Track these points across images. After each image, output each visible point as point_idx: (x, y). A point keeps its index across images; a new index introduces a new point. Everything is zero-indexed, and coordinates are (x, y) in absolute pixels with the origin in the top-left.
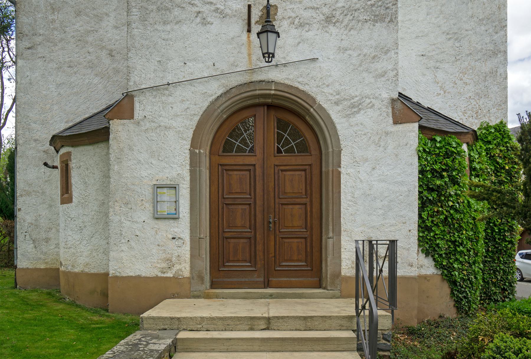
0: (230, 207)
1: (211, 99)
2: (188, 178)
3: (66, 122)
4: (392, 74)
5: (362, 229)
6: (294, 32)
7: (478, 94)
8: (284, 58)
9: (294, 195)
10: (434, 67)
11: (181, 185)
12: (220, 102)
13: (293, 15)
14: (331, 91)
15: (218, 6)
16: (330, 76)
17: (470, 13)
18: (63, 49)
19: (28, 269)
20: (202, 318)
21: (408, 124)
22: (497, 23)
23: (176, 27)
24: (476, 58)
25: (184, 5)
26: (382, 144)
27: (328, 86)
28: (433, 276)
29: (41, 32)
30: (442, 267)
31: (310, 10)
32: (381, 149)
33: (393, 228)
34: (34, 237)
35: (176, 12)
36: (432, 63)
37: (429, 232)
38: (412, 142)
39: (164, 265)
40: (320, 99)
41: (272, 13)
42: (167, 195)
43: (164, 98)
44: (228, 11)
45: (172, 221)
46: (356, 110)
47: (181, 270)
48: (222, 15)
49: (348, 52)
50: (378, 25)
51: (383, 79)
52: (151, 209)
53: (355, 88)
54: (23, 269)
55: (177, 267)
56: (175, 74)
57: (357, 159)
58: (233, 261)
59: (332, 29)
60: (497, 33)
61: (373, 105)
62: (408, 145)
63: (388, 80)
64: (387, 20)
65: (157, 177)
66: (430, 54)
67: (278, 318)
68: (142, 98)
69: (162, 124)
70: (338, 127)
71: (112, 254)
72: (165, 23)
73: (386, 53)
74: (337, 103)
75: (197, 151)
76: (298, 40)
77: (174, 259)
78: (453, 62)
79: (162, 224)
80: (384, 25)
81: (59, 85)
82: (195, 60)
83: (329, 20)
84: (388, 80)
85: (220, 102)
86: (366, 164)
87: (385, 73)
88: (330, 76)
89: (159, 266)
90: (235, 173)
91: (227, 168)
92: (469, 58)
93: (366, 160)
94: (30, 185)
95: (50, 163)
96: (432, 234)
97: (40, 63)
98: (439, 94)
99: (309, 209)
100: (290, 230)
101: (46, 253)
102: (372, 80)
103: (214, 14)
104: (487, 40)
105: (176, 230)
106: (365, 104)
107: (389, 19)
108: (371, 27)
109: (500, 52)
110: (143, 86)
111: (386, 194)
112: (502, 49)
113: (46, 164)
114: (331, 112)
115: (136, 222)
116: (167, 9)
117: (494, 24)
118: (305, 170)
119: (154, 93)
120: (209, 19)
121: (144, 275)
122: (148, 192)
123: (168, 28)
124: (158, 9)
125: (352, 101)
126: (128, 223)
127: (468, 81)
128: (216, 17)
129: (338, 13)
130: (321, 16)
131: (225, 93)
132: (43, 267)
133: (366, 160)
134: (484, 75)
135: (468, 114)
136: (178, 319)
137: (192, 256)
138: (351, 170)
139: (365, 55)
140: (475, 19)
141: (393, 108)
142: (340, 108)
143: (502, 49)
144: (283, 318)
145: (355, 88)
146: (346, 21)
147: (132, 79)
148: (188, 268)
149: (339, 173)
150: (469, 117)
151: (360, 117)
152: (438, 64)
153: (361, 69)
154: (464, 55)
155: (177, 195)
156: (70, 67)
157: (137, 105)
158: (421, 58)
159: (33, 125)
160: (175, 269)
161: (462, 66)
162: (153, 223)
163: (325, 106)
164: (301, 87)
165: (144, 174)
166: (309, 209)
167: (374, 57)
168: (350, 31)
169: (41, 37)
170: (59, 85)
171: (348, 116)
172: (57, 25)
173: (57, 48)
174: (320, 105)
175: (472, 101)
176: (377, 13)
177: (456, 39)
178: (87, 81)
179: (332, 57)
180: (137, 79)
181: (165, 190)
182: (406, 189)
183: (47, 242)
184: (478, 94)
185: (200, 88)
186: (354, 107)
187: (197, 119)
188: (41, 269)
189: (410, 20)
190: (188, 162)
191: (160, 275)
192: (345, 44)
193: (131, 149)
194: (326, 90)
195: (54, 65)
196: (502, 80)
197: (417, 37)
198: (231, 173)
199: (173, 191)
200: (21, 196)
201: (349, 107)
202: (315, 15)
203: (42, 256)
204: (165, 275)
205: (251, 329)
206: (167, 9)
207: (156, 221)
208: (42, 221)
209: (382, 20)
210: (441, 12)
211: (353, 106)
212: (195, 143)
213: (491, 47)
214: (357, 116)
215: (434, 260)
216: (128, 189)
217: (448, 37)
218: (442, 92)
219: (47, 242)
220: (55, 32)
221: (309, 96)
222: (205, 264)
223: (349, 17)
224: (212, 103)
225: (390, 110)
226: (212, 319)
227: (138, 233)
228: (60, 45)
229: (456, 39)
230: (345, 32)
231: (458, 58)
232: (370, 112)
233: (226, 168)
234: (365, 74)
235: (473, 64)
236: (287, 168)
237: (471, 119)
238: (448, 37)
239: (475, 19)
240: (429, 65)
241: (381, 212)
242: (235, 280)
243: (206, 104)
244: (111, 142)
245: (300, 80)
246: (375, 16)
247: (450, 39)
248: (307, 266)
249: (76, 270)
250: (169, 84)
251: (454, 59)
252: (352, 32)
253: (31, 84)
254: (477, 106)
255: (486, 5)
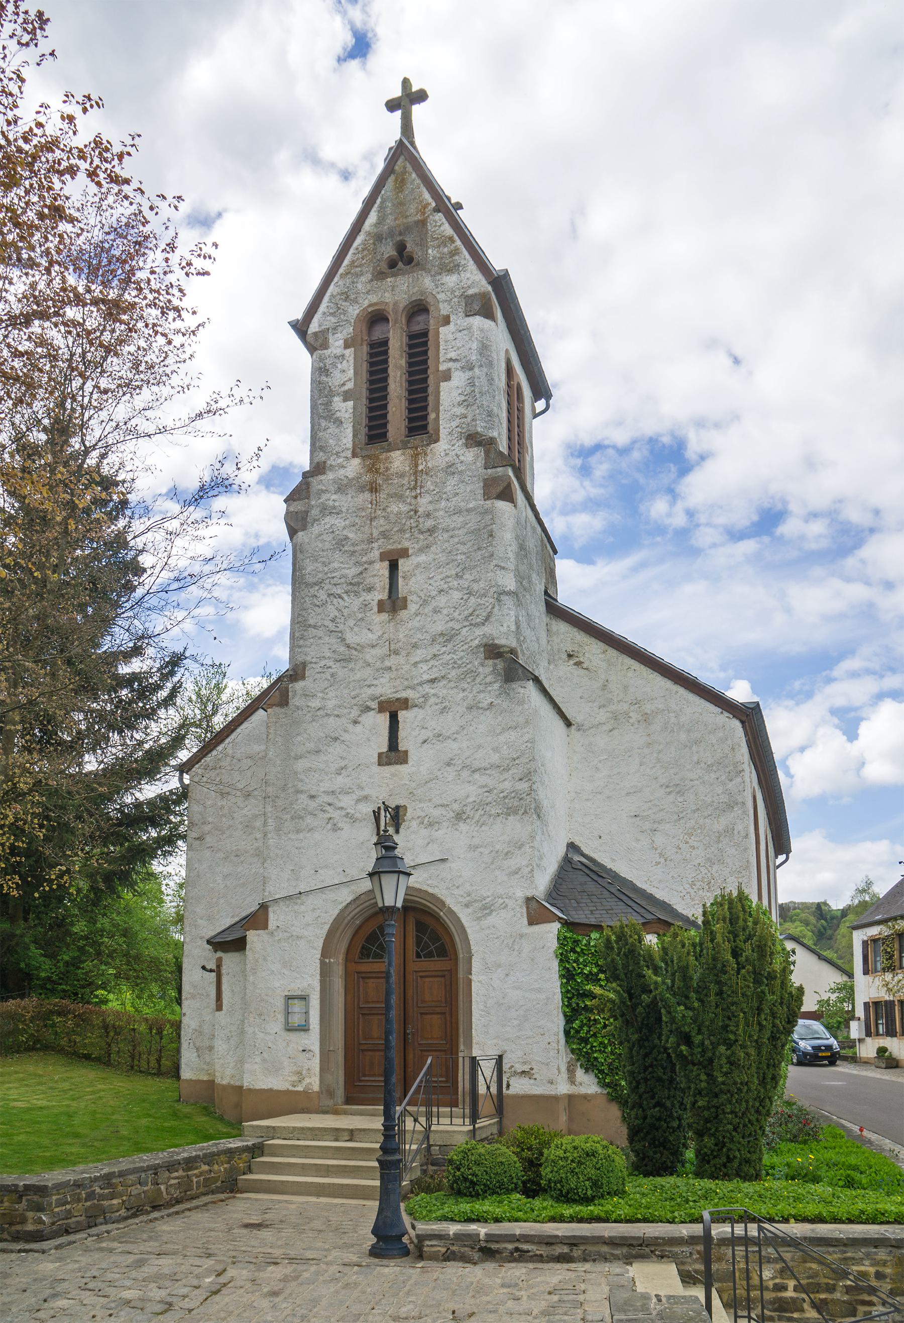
0: (367, 1017)
1: (340, 907)
2: (318, 989)
3: (233, 917)
4: (526, 870)
5: (495, 1041)
6: (423, 832)
7: (709, 860)
8: (414, 860)
9: (433, 1004)
10: (651, 830)
11: (311, 996)
12: (349, 910)
13: (423, 814)
14: (462, 893)
15: (349, 811)
16: (460, 876)
17: (695, 758)
18: (231, 836)
19: (191, 1080)
20: (294, 1128)
21: (545, 925)
22: (731, 768)
23: (309, 835)
24: (706, 814)
25: (316, 812)
26: (516, 947)
27: (458, 887)
28: (594, 1096)
29: (210, 819)
30: (608, 1085)
31: (440, 808)
32: (515, 953)
33: (530, 1041)
34: (198, 1044)
35: (309, 820)
36: (647, 825)
37: (587, 1044)
38: (549, 945)
39: (295, 1078)
40: (450, 902)
41: (401, 813)
42: (297, 1006)
43: (296, 907)
44: (358, 815)
45: (302, 1033)
46: (487, 911)
47: (310, 1084)
48: (352, 819)
49: (479, 850)
50: (511, 818)
51: (517, 876)
52: (283, 1020)
53: (486, 888)
54: (186, 1080)
55: (307, 1080)
56: (308, 882)
57: (490, 965)
58: (369, 1076)
59: (463, 827)
60: (731, 780)
61: (507, 905)
62: (546, 948)
63: (523, 877)
64: (521, 812)
65: (289, 988)
66: (646, 814)
67: (361, 1130)
68: (276, 908)
69: (294, 934)
70: (469, 931)
71: (247, 1066)
72: (298, 831)
73: (520, 848)
74: (467, 906)
75: (327, 961)
76: (428, 840)
77: (304, 1072)
78: (676, 821)
79: (294, 1036)
80: (518, 817)
81: (225, 877)
82: (326, 867)
83: (459, 817)
84: (523, 877)
85: (349, 910)
86: (499, 970)
87: (520, 869)
88: (460, 876)
89: (290, 1079)
90: (372, 980)
91: (363, 975)
92: (696, 815)
93: (499, 966)
94: (195, 987)
95: (208, 967)
96: (589, 1047)
97: (207, 853)
98: (658, 863)
99: (448, 1019)
100: (430, 1042)
101: (209, 1063)
102: (505, 878)
103: (345, 819)
104: (720, 790)
105: (306, 1042)
106: (497, 905)
107: (523, 811)
108: (504, 820)
109: (737, 804)
110: (277, 896)
111: (521, 1003)
112: (740, 800)
113: (204, 968)
114: (461, 915)
115: (269, 1034)
116: (301, 818)
117: (727, 770)
118: (444, 976)
119: (288, 902)
120: (340, 825)
121: (275, 1088)
122: (280, 1003)
123: (301, 836)
124: (292, 818)
125: (484, 902)
126: (262, 1034)
127: (695, 844)
128: (346, 822)
129: (469, 809)
130: (451, 813)
131: (354, 900)
132: (205, 1078)
133: (499, 966)
134: (717, 834)
135: (698, 886)
136: (274, 1127)
137: (322, 1070)
138: (482, 978)
139: (497, 852)
140: (702, 765)
141: (528, 908)
142: (470, 910)
143: (740, 800)
144: (364, 1130)
145: (486, 888)
146: (477, 817)
147: (268, 889)
148: (318, 1082)
149: (470, 981)
150: (699, 889)
151: (491, 920)
152: (656, 826)
153: (493, 867)
154: (689, 811)
155: (307, 1007)
156: (237, 856)
157: (271, 916)
158: (634, 819)
159: (200, 921)
160: (305, 1083)
161: (687, 826)
162: (285, 1034)
163: (455, 909)
164: (431, 890)
165: (277, 984)
166: (448, 1019)
167: (507, 854)
168: (481, 827)
169: (210, 826)
170: (225, 877)
171: (479, 919)
172: (226, 811)
173: (225, 836)
174: (450, 908)
175: (702, 869)
176: (510, 805)
177: (678, 793)
178: (253, 871)
179: (462, 856)
180: (272, 888)
181: (296, 1001)
182: (544, 997)
183: (210, 1051)
184: (709, 860)
185: (330, 895)
186: (485, 909)
187: (327, 927)
188: (203, 1081)
189: (619, 773)
190: (319, 972)
191: (291, 1088)
192: (476, 841)
193: (265, 960)
194: (456, 892)
195: (221, 855)
196: (740, 839)
197: (628, 794)
198: (367, 981)
199: (303, 1003)
200: (186, 999)
201: (480, 909)
202: (444, 813)
203: (206, 1067)
204: (296, 1089)
205: (336, 1140)
206: (301, 818)
207: (288, 1033)
208: (205, 1027)
209: (516, 812)
210: (658, 760)
211: (484, 908)
212: (326, 952)
213: (724, 798)
214: (489, 918)
215: (596, 1076)
216: (262, 1000)
217: (668, 790)
218: (662, 860)
219: (210, 1051)
220: (224, 819)
221: (438, 899)
222: (338, 1078)
223: (481, 812)
224: (342, 911)
225: (525, 910)
226: (303, 1129)
227: (270, 1045)
228: (228, 832)
229: (678, 793)
230: (476, 829)
231: (681, 815)
232: (503, 913)
233: (364, 976)
234: (497, 873)
235: (701, 821)
236: (426, 974)
237: (701, 892)
238: (668, 790)
239: (702, 765)
240: (644, 828)
241: (516, 1022)
242: (371, 1095)
243: (336, 912)
244: (247, 952)
245: (430, 882)
246: (508, 809)
247: (669, 793)
248: (446, 1082)
249: (224, 1082)
250: (300, 893)
251: (676, 817)
252: (484, 828)
253: (198, 876)
254: (709, 875)
255: (716, 747)
